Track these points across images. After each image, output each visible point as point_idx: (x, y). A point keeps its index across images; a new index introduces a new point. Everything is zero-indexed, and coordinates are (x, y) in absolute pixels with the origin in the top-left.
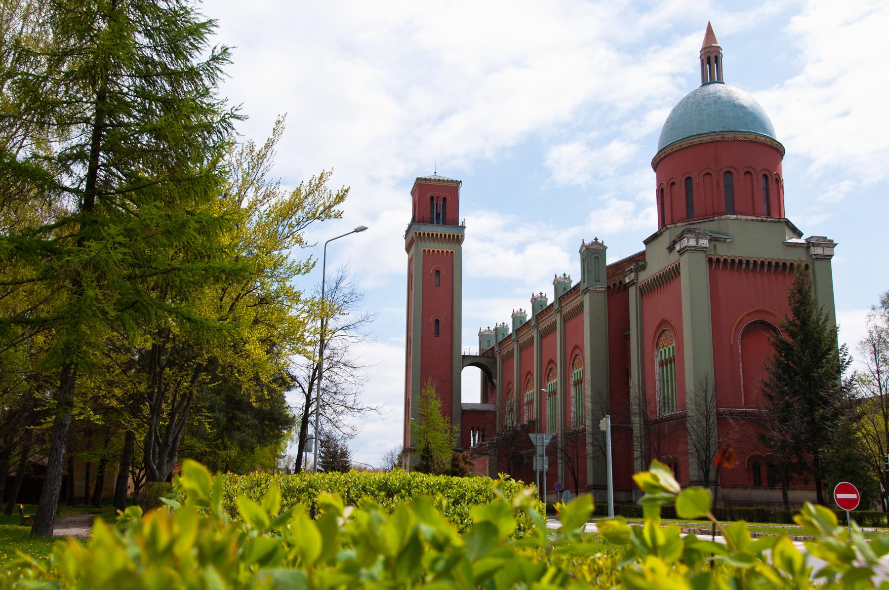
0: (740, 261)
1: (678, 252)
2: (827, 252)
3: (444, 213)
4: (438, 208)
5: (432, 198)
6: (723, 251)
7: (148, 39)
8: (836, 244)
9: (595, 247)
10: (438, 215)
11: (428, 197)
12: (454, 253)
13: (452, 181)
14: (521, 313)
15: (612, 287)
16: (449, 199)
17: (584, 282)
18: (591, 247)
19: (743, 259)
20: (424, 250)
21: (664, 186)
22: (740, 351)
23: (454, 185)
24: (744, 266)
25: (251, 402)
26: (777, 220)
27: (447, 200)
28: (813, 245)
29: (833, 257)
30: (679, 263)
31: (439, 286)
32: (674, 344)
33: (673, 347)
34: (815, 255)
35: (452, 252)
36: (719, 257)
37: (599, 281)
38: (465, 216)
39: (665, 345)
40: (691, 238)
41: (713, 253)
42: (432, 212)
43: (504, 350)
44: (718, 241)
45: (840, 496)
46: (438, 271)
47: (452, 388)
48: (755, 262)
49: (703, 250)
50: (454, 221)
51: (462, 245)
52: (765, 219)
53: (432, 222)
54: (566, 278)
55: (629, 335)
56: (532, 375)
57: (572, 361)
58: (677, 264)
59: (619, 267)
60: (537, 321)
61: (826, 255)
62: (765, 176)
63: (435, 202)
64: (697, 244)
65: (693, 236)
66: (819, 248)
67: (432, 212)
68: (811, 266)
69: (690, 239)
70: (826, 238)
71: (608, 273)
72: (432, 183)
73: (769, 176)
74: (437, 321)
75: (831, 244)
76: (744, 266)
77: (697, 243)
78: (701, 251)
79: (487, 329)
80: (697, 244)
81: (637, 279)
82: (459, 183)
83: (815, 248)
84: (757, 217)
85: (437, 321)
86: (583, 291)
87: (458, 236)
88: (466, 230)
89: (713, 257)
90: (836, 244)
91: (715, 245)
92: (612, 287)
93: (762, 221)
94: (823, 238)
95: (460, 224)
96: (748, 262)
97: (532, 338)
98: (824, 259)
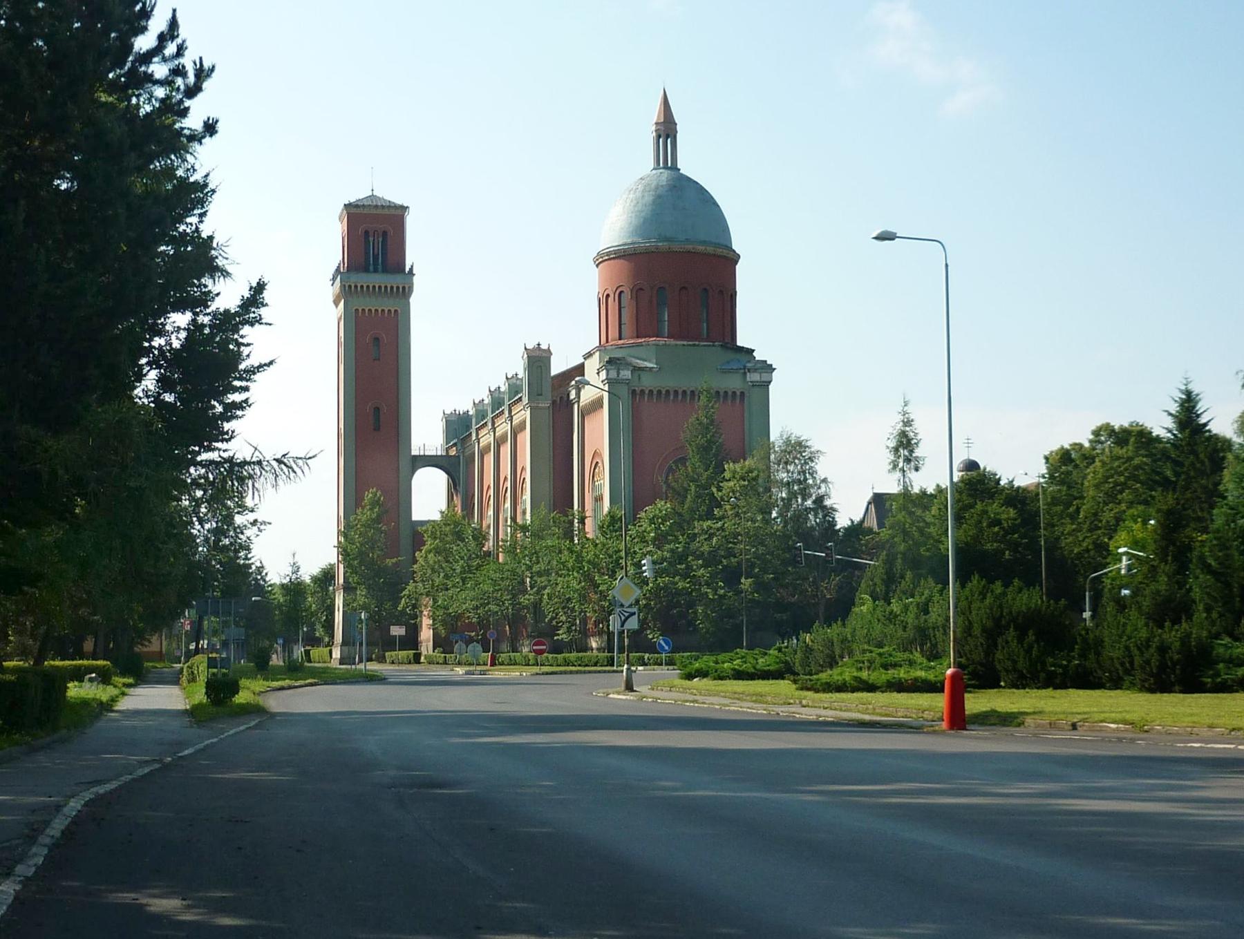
0: (668, 392)
2: (765, 377)
4: (376, 250)
5: (367, 233)
6: (647, 382)
7: (206, 697)
9: (538, 353)
10: (376, 258)
12: (399, 312)
16: (391, 232)
20: (357, 310)
21: (601, 296)
23: (399, 212)
28: (749, 371)
31: (379, 359)
35: (396, 311)
37: (541, 395)
42: (367, 253)
45: (545, 647)
46: (377, 339)
47: (401, 498)
49: (627, 382)
51: (412, 300)
52: (697, 343)
53: (366, 270)
54: (518, 379)
61: (763, 382)
67: (367, 253)
70: (766, 361)
72: (366, 211)
74: (377, 409)
81: (579, 398)
82: (404, 209)
85: (377, 409)
87: (404, 288)
88: (415, 278)
91: (639, 375)
95: (407, 269)
97: (524, 421)
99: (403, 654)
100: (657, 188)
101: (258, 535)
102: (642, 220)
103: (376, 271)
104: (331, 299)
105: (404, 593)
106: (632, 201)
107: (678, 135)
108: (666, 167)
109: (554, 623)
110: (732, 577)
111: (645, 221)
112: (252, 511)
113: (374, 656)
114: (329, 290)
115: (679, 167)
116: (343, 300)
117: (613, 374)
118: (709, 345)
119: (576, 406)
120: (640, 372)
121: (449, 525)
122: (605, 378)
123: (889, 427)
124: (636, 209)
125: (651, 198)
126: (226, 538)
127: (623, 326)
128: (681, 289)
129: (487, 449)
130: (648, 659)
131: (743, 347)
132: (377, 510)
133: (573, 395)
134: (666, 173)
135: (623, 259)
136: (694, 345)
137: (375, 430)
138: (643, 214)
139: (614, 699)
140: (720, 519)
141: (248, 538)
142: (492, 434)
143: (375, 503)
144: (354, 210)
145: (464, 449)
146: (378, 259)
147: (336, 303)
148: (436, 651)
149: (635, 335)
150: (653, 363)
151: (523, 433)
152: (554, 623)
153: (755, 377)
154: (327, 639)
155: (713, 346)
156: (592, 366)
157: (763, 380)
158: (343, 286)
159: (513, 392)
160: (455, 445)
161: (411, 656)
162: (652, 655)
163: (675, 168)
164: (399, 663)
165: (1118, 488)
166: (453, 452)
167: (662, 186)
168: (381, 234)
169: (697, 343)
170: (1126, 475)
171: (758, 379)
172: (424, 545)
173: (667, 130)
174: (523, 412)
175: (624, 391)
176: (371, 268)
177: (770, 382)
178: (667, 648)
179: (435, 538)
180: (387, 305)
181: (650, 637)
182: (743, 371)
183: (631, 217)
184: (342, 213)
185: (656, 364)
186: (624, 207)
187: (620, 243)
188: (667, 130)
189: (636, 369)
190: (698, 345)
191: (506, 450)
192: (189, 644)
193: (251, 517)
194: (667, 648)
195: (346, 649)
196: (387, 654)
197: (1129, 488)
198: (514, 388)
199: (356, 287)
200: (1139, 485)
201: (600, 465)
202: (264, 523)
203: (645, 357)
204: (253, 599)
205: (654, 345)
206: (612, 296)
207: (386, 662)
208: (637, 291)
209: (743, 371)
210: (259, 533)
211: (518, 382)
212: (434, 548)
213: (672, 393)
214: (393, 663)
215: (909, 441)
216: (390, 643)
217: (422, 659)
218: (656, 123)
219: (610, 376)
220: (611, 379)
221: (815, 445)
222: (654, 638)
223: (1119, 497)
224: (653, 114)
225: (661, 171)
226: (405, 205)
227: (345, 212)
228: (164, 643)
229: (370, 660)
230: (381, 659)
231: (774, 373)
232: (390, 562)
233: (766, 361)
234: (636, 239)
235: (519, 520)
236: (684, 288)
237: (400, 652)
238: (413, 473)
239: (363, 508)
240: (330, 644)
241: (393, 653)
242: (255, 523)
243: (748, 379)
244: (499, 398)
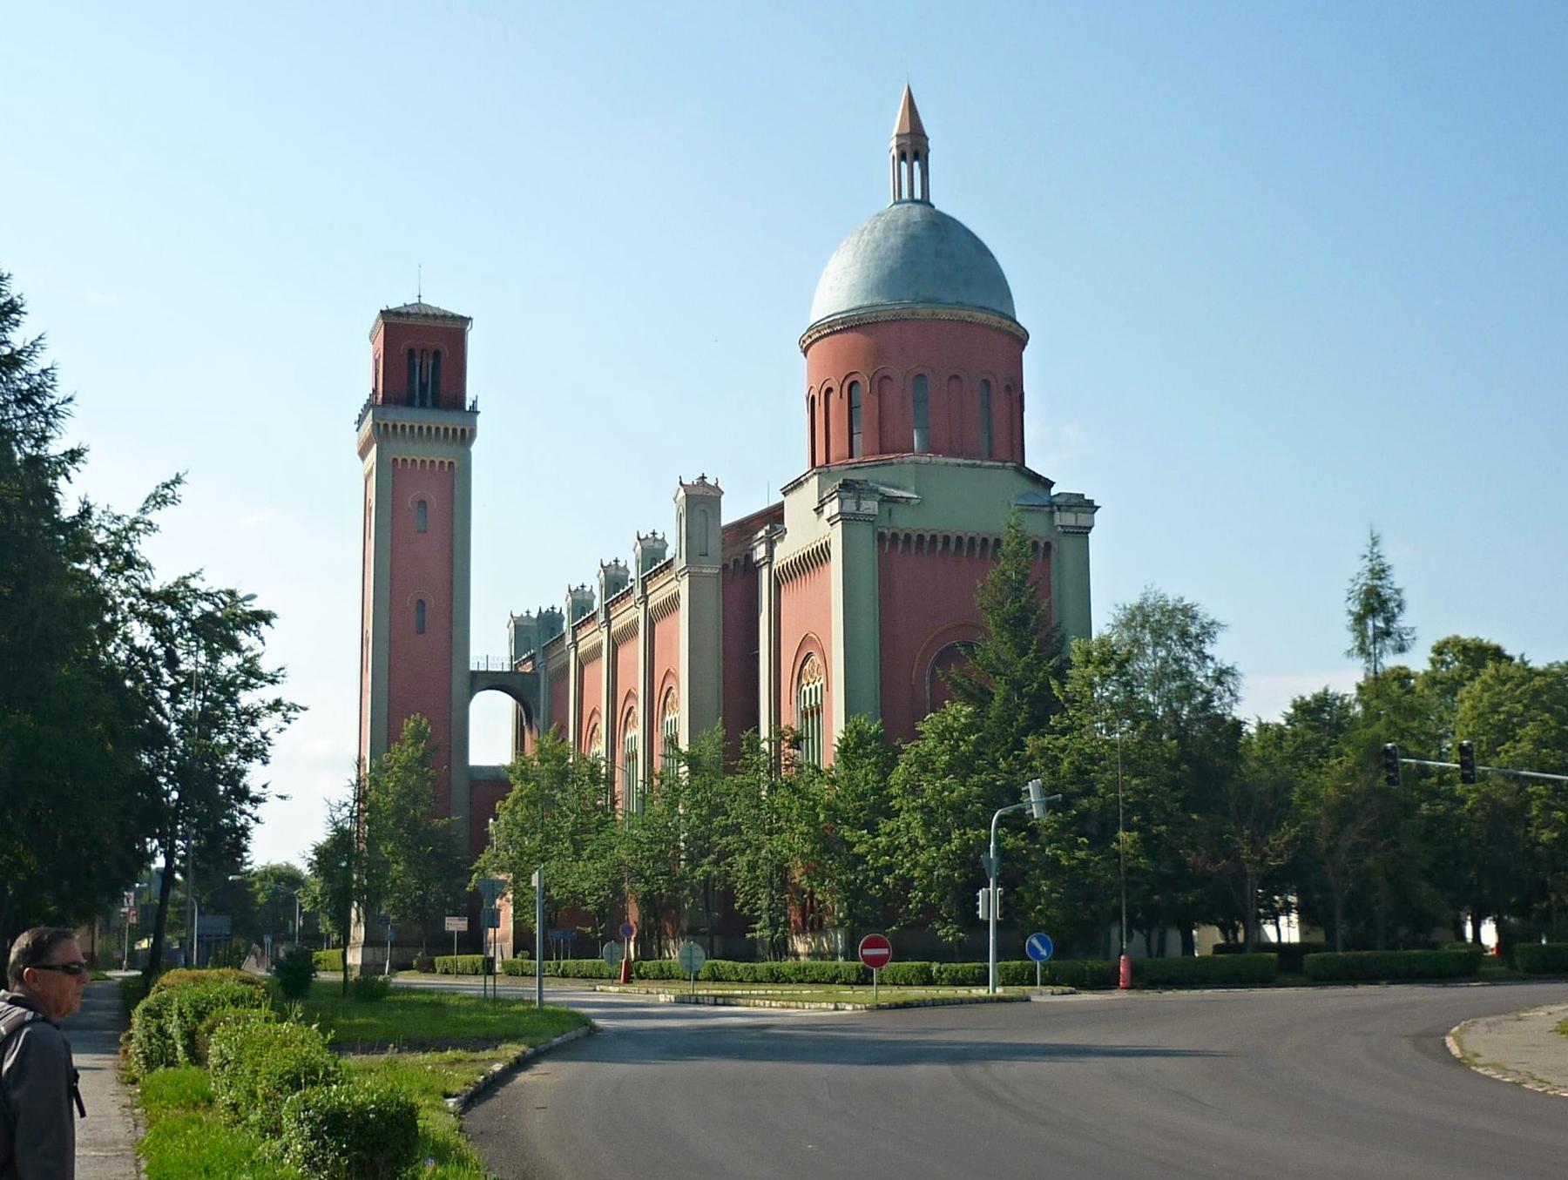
2: (1083, 520)
3: (435, 383)
5: (411, 353)
6: (904, 521)
8: (1098, 508)
10: (423, 386)
12: (456, 465)
13: (454, 318)
14: (584, 593)
16: (446, 353)
21: (815, 392)
23: (458, 325)
24: (940, 546)
25: (124, 896)
26: (1000, 464)
28: (1059, 510)
31: (425, 532)
34: (1062, 526)
35: (451, 463)
36: (896, 531)
37: (706, 555)
39: (811, 681)
42: (411, 381)
43: (552, 662)
44: (896, 502)
46: (422, 503)
47: (455, 734)
48: (959, 539)
49: (869, 519)
52: (979, 462)
54: (656, 540)
55: (758, 654)
56: (600, 716)
57: (662, 699)
59: (746, 528)
60: (608, 613)
61: (1080, 527)
63: (418, 361)
64: (858, 509)
65: (850, 495)
66: (1069, 514)
67: (411, 381)
68: (1055, 545)
70: (1083, 495)
71: (723, 539)
72: (412, 321)
73: (993, 384)
75: (1090, 507)
76: (940, 546)
79: (525, 614)
80: (858, 509)
82: (465, 321)
83: (1063, 514)
84: (965, 459)
87: (463, 431)
88: (479, 418)
89: (886, 531)
90: (1098, 508)
91: (890, 511)
92: (732, 567)
93: (973, 466)
94: (1078, 495)
95: (468, 404)
96: (947, 539)
97: (600, 646)
98: (1077, 533)
99: (465, 960)
100: (907, 225)
101: (281, 730)
102: (886, 272)
103: (423, 405)
104: (356, 449)
105: (477, 864)
106: (867, 244)
107: (930, 155)
108: (913, 200)
109: (745, 910)
110: (1101, 830)
111: (892, 271)
112: (273, 682)
113: (415, 962)
114: (352, 438)
115: (932, 201)
116: (375, 446)
117: (850, 506)
118: (998, 467)
119: (765, 571)
120: (890, 505)
121: (548, 761)
122: (836, 511)
123: (1351, 572)
124: (876, 254)
125: (899, 240)
126: (220, 733)
127: (855, 436)
128: (951, 378)
129: (595, 653)
130: (939, 971)
131: (1041, 476)
132: (423, 745)
133: (760, 552)
134: (917, 210)
135: (857, 331)
136: (973, 466)
137: (417, 632)
138: (889, 262)
139: (409, 990)
140: (1063, 732)
141: (264, 735)
142: (643, 606)
143: (418, 736)
144: (394, 320)
145: (547, 662)
146: (426, 391)
147: (363, 454)
148: (519, 955)
149: (878, 449)
150: (910, 492)
151: (673, 617)
152: (745, 910)
153: (1068, 519)
154: (335, 937)
155: (1004, 467)
156: (799, 509)
157: (1079, 524)
158: (376, 426)
159: (579, 610)
160: (531, 658)
161: (480, 963)
162: (946, 965)
163: (925, 201)
164: (458, 973)
165: (1515, 720)
166: (527, 668)
167: (915, 223)
168: (431, 354)
169: (979, 462)
170: (1525, 701)
171: (1073, 523)
172: (511, 791)
173: (914, 147)
174: (675, 583)
175: (865, 535)
176: (417, 402)
177: (1090, 528)
178: (1044, 953)
179: (527, 781)
181: (940, 933)
182: (1048, 509)
183: (868, 267)
184: (377, 321)
185: (917, 493)
186: (855, 254)
187: (853, 306)
188: (914, 147)
189: (886, 500)
190: (979, 466)
191: (633, 653)
192: (134, 943)
193: (267, 694)
194: (1044, 953)
195: (369, 950)
196: (437, 959)
197: (1533, 720)
198: (653, 557)
199: (395, 427)
200: (1547, 715)
201: (816, 658)
202: (294, 707)
203: (897, 483)
204: (230, 878)
205: (911, 462)
206: (836, 390)
207: (435, 971)
208: (879, 382)
209: (1048, 509)
210: (285, 725)
211: (657, 545)
212: (526, 796)
213: (940, 540)
214: (447, 972)
215: (1384, 603)
216: (443, 943)
217: (498, 967)
218: (898, 136)
219: (845, 509)
220: (848, 514)
221: (1208, 609)
222: (947, 935)
223: (1520, 732)
224: (896, 122)
225: (906, 205)
227: (381, 321)
228: (98, 942)
229: (408, 967)
230: (429, 968)
232: (438, 823)
233: (1083, 495)
234: (877, 300)
236: (956, 377)
237: (459, 957)
238: (471, 696)
239: (401, 743)
240: (344, 942)
241: (448, 958)
242: (276, 706)
243: (1057, 521)
244: (615, 576)
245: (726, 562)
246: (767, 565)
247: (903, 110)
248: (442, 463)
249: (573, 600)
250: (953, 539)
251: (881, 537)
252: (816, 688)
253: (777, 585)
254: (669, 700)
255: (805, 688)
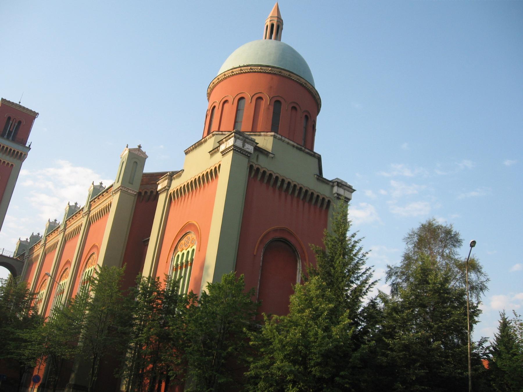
1: (222, 152)
5: (9, 118)
6: (263, 163)
9: (136, 152)
10: (10, 133)
11: (6, 116)
12: (14, 166)
15: (143, 194)
17: (118, 182)
18: (134, 152)
19: (279, 177)
22: (261, 263)
23: (32, 114)
27: (22, 124)
29: (351, 200)
30: (220, 165)
32: (195, 247)
33: (193, 250)
35: (12, 165)
36: (260, 167)
37: (132, 184)
38: (33, 138)
40: (238, 138)
41: (256, 163)
50: (23, 141)
58: (217, 166)
62: (306, 117)
63: (11, 122)
69: (238, 140)
75: (351, 190)
77: (244, 146)
78: (245, 154)
80: (243, 146)
86: (114, 191)
89: (254, 165)
90: (354, 190)
92: (143, 194)
95: (27, 145)
168: (17, 122)
176: (5, 137)
180: (7, 159)
226: (37, 112)
231: (353, 194)
235: (89, 275)
245: (141, 191)
246: (166, 191)
247: (275, 7)
248: (8, 164)
249: (49, 225)
250: (286, 182)
251: (251, 167)
252: (183, 254)
253: (170, 200)
254: (90, 261)
255: (180, 253)
